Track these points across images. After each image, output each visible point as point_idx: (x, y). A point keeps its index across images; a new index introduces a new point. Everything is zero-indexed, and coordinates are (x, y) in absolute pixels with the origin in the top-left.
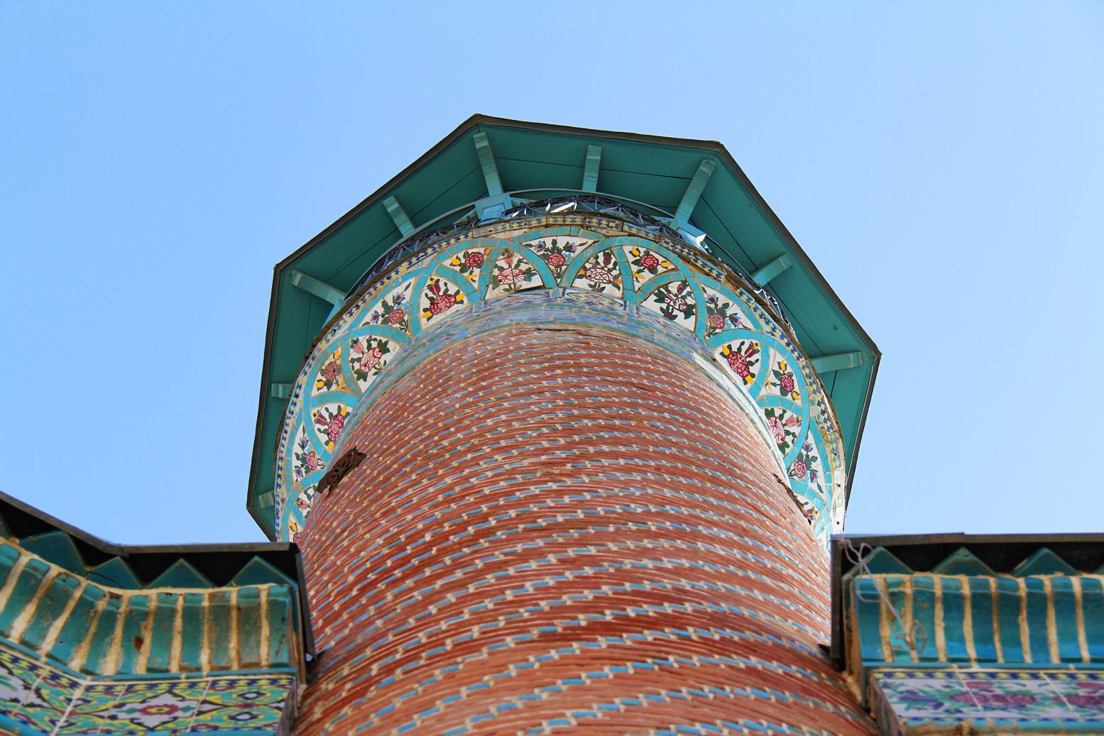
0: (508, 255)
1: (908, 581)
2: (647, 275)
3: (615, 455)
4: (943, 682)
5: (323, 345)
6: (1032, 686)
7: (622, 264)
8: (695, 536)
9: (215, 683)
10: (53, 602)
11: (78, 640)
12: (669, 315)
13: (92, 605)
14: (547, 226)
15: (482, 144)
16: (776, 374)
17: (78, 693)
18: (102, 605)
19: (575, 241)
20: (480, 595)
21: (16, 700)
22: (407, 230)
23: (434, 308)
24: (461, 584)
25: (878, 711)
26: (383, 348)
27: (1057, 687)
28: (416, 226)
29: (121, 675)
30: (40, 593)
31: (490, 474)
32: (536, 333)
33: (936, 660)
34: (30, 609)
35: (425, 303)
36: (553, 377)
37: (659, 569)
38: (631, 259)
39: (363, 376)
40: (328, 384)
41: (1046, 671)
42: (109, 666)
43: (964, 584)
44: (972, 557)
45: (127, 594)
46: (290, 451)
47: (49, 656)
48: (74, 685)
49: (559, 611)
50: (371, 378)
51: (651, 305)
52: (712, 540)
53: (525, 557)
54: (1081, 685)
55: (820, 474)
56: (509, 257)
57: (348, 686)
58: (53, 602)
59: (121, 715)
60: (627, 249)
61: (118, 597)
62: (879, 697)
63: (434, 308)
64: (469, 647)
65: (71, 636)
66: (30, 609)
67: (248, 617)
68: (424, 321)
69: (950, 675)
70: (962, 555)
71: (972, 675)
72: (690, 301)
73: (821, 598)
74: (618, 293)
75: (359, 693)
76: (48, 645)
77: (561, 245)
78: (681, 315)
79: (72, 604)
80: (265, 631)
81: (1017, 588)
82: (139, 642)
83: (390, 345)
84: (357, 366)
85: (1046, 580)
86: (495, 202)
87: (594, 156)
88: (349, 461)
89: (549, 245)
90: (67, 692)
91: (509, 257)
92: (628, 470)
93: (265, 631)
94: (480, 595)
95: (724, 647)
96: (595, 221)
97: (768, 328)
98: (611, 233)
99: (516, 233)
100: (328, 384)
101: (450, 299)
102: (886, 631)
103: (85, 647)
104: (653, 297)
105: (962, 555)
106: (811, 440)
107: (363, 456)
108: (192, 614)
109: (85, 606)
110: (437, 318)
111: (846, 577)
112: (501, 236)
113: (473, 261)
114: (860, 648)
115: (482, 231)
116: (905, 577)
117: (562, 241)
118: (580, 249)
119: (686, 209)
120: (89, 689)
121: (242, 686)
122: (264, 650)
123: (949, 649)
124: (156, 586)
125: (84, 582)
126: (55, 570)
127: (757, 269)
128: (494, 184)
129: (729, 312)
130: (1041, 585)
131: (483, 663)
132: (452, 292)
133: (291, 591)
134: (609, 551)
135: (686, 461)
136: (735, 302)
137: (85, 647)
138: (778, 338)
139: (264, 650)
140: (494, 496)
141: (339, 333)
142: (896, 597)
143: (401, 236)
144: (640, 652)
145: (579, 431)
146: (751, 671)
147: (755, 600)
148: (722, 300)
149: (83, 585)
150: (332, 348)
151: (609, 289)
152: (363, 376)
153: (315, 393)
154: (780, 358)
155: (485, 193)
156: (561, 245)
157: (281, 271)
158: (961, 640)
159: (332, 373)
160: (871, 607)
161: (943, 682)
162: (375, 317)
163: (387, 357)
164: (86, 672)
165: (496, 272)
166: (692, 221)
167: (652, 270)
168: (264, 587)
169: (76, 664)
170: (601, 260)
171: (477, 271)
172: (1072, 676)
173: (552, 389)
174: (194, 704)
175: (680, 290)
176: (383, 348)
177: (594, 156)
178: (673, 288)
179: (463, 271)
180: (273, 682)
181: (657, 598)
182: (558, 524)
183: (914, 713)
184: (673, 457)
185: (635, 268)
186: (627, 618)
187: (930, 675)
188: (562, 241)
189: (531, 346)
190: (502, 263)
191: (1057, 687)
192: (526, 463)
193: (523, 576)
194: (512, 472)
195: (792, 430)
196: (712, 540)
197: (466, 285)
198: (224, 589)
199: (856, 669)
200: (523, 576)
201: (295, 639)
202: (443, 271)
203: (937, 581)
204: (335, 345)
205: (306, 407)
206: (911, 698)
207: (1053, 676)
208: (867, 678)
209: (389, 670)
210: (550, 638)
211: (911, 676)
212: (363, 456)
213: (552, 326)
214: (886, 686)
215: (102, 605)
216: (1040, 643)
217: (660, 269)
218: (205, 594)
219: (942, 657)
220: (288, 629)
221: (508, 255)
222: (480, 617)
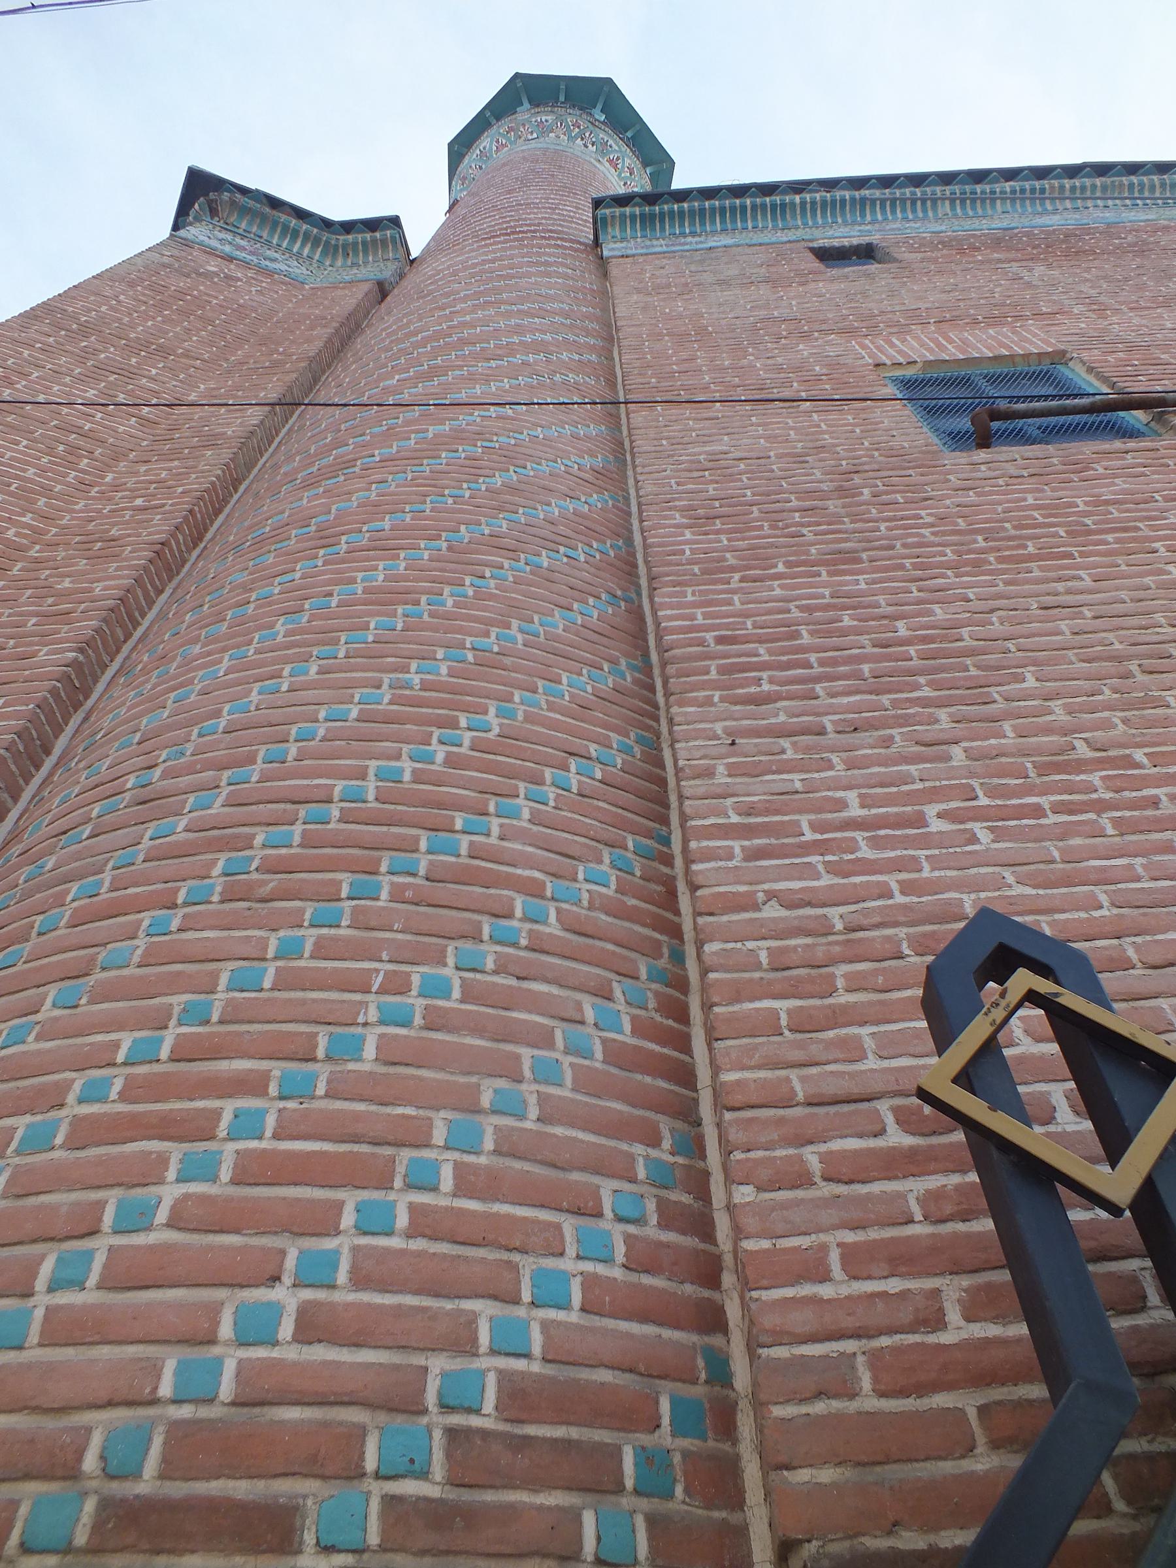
0: (524, 125)
1: (618, 211)
7: (567, 126)
10: (295, 234)
12: (586, 147)
18: (333, 242)
19: (549, 118)
34: (309, 245)
41: (1147, 750)
43: (637, 210)
45: (341, 238)
58: (316, 242)
70: (637, 200)
85: (666, 207)
86: (526, 105)
102: (610, 230)
105: (637, 200)
108: (364, 243)
109: (327, 243)
113: (511, 129)
126: (315, 231)
149: (325, 236)
215: (333, 242)
218: (368, 236)
221: (524, 125)
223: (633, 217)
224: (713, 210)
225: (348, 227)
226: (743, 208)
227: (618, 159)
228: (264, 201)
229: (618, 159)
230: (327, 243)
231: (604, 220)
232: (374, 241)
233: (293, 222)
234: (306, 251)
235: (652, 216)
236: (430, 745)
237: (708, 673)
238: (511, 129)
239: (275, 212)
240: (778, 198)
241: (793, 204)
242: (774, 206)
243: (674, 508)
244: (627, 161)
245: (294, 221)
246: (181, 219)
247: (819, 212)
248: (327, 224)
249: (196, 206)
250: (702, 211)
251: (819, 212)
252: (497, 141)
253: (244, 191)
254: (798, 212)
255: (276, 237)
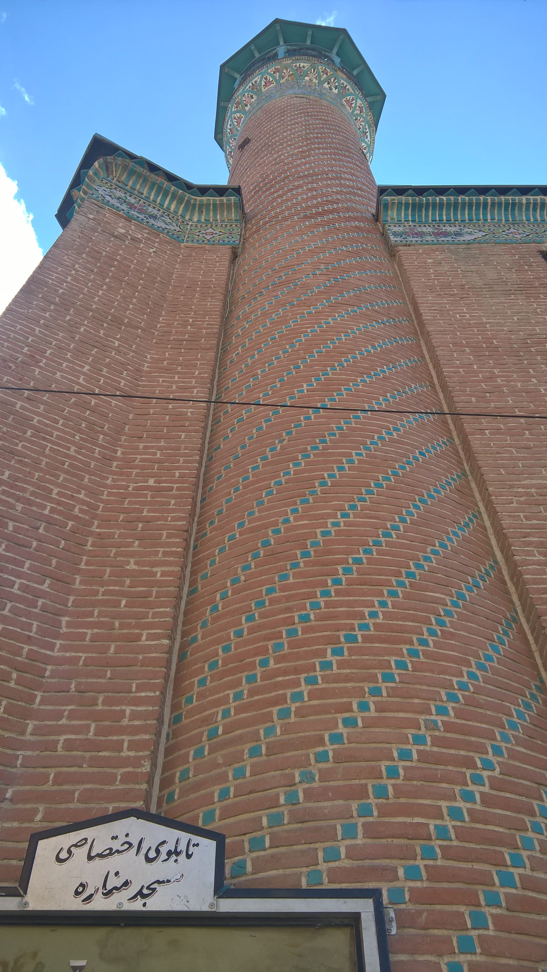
1: (397, 199)
2: (325, 76)
3: (319, 149)
4: (403, 228)
5: (236, 95)
6: (424, 229)
7: (318, 72)
8: (341, 178)
9: (222, 225)
11: (187, 211)
12: (331, 89)
13: (190, 202)
14: (298, 59)
15: (278, 28)
16: (359, 107)
17: (189, 227)
19: (305, 65)
20: (287, 200)
21: (175, 230)
22: (257, 55)
23: (266, 85)
24: (280, 196)
25: (386, 235)
26: (252, 98)
27: (430, 230)
28: (260, 54)
29: (199, 221)
30: (177, 198)
31: (286, 154)
32: (295, 99)
33: (401, 221)
34: (175, 202)
35: (263, 83)
36: (301, 117)
37: (332, 192)
38: (321, 71)
39: (246, 105)
40: (237, 107)
42: (195, 219)
44: (413, 192)
45: (198, 198)
46: (227, 127)
47: (181, 215)
48: (188, 224)
49: (308, 207)
50: (249, 106)
51: (326, 85)
52: (346, 179)
53: (297, 187)
54: (436, 229)
55: (369, 136)
56: (287, 69)
57: (255, 227)
59: (200, 235)
60: (320, 67)
61: (196, 199)
62: (387, 233)
63: (266, 85)
64: (285, 219)
65: (186, 209)
66: (175, 202)
67: (229, 206)
68: (263, 89)
69: (404, 226)
70: (410, 191)
71: (410, 226)
72: (337, 84)
73: (372, 195)
74: (317, 82)
75: (257, 231)
76: (180, 212)
77: (301, 66)
78: (334, 89)
79: (185, 201)
80: (233, 210)
81: (423, 201)
82: (202, 212)
83: (254, 96)
84: (245, 102)
85: (430, 198)
87: (310, 33)
88: (247, 141)
89: (298, 66)
90: (186, 226)
91: (287, 69)
92: (323, 154)
93: (233, 210)
94: (287, 200)
95: (349, 219)
96: (311, 58)
97: (357, 93)
98: (316, 62)
99: (289, 62)
100: (237, 107)
101: (270, 82)
102: (390, 213)
103: (189, 213)
104: (327, 83)
105: (410, 191)
106: (367, 127)
107: (249, 140)
108: (215, 205)
109: (188, 202)
110: (266, 88)
111: (381, 197)
112: (284, 62)
113: (277, 70)
114: (382, 217)
115: (279, 61)
116: (396, 198)
117: (302, 65)
118: (307, 67)
119: (335, 51)
120: (192, 225)
121: (228, 227)
122: (233, 216)
123: (405, 218)
124: (205, 197)
125: (188, 195)
126: (180, 191)
127: (354, 69)
128: (282, 42)
129: (347, 88)
130: (429, 200)
131: (289, 225)
132: (271, 80)
133: (239, 199)
134: (319, 185)
135: (338, 149)
136: (349, 84)
137: (189, 213)
138: (360, 96)
139: (233, 216)
140: (288, 164)
141: (240, 92)
142: (393, 204)
143: (255, 57)
144: (328, 223)
145: (309, 139)
146: (356, 227)
147: (356, 200)
148: (345, 84)
150: (238, 96)
151: (314, 80)
152: (246, 105)
153: (233, 110)
154: (360, 102)
155: (279, 44)
156: (301, 66)
157: (222, 67)
158: (408, 215)
159: (238, 104)
160: (386, 206)
161: (403, 228)
162: (250, 87)
163: (253, 100)
164: (190, 220)
165: (283, 74)
166: (337, 54)
167: (327, 74)
168: (232, 198)
169: (187, 218)
170: (312, 71)
171: (278, 74)
172: (434, 226)
173: (301, 122)
174: (217, 232)
175: (334, 81)
176: (252, 98)
177: (310, 33)
178: (332, 80)
179: (274, 73)
180: (236, 225)
181: (332, 202)
182: (306, 175)
183: (395, 239)
184: (335, 148)
185: (322, 74)
186: (325, 210)
187: (400, 226)
188: (302, 65)
189: (294, 104)
190: (285, 71)
191: (430, 230)
192: (296, 151)
193: (297, 195)
194: (293, 155)
195: (362, 124)
196: (346, 179)
197: (274, 78)
198: (222, 198)
199: (381, 221)
200: (297, 195)
201: (240, 212)
202: (269, 74)
203: (403, 198)
204: (238, 96)
205: (231, 114)
206: (395, 234)
207: (429, 226)
208: (384, 226)
209: (265, 224)
210: (306, 217)
211: (395, 226)
212: (249, 140)
213: (299, 96)
214: (389, 230)
215: (192, 202)
216: (427, 216)
217: (329, 74)
219: (403, 220)
220: (239, 209)
222: (288, 208)
223: (407, 205)
224: (464, 204)
225: (203, 190)
226: (485, 204)
227: (353, 100)
228: (146, 166)
229: (353, 100)
230: (188, 202)
231: (386, 206)
232: (222, 205)
233: (166, 184)
234: (173, 207)
235: (420, 205)
236: (23, 568)
237: (174, 378)
238: (277, 70)
239: (152, 175)
240: (510, 198)
241: (521, 204)
242: (507, 204)
243: (529, 544)
244: (359, 102)
245: (166, 183)
246: (82, 171)
247: (538, 211)
248: (188, 187)
249: (96, 164)
250: (456, 204)
251: (538, 211)
252: (266, 79)
253: (132, 157)
254: (524, 210)
255: (153, 194)
